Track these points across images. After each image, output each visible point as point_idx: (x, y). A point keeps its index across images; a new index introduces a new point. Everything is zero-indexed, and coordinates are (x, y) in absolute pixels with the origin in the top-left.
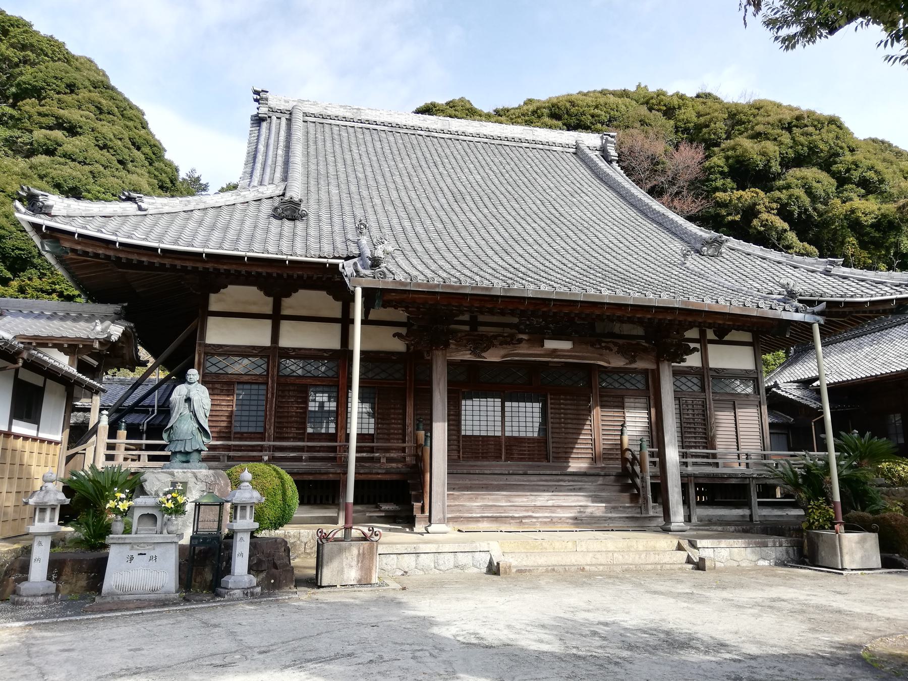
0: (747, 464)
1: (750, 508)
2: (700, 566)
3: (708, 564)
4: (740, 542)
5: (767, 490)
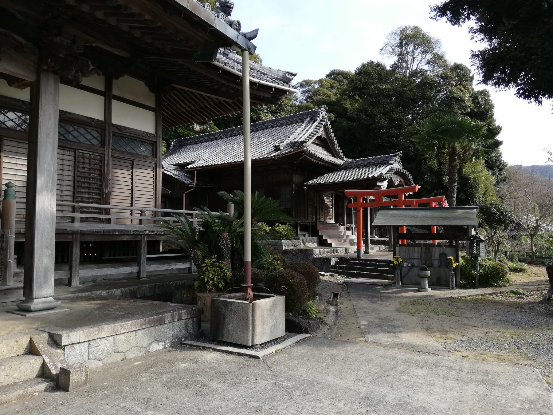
0: (141, 220)
1: (139, 266)
2: (58, 382)
3: (74, 378)
4: (128, 325)
5: (153, 246)
